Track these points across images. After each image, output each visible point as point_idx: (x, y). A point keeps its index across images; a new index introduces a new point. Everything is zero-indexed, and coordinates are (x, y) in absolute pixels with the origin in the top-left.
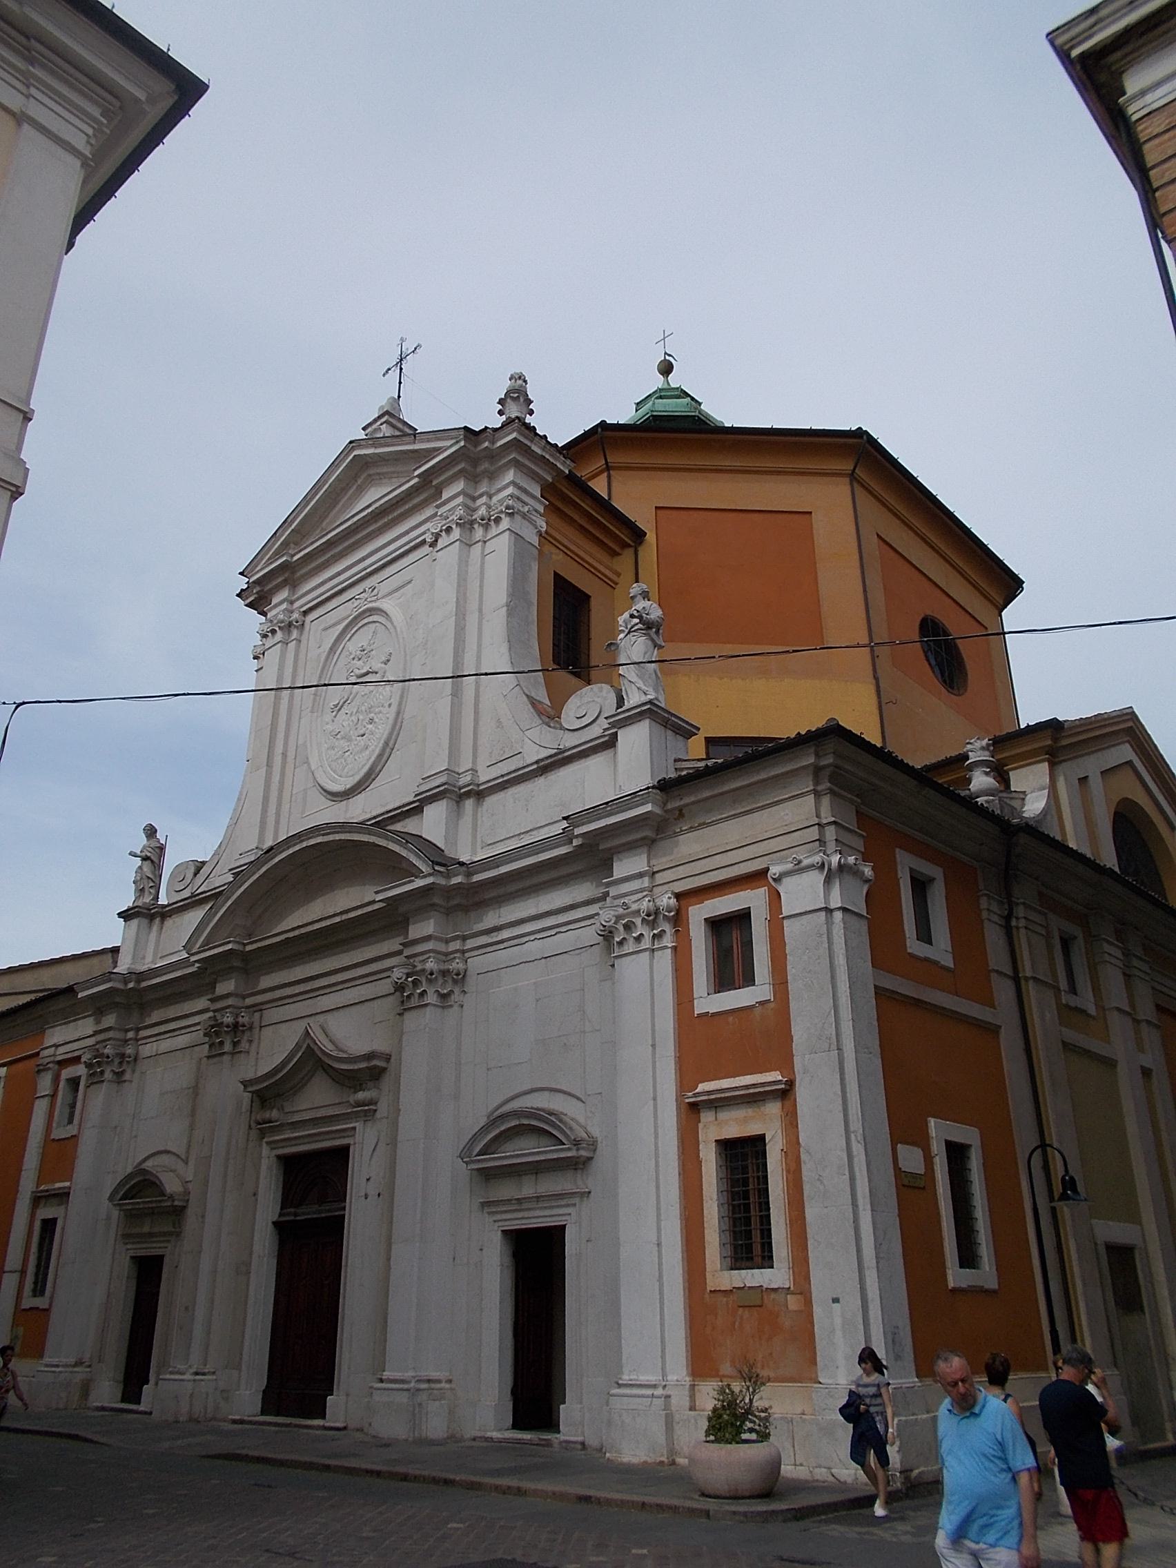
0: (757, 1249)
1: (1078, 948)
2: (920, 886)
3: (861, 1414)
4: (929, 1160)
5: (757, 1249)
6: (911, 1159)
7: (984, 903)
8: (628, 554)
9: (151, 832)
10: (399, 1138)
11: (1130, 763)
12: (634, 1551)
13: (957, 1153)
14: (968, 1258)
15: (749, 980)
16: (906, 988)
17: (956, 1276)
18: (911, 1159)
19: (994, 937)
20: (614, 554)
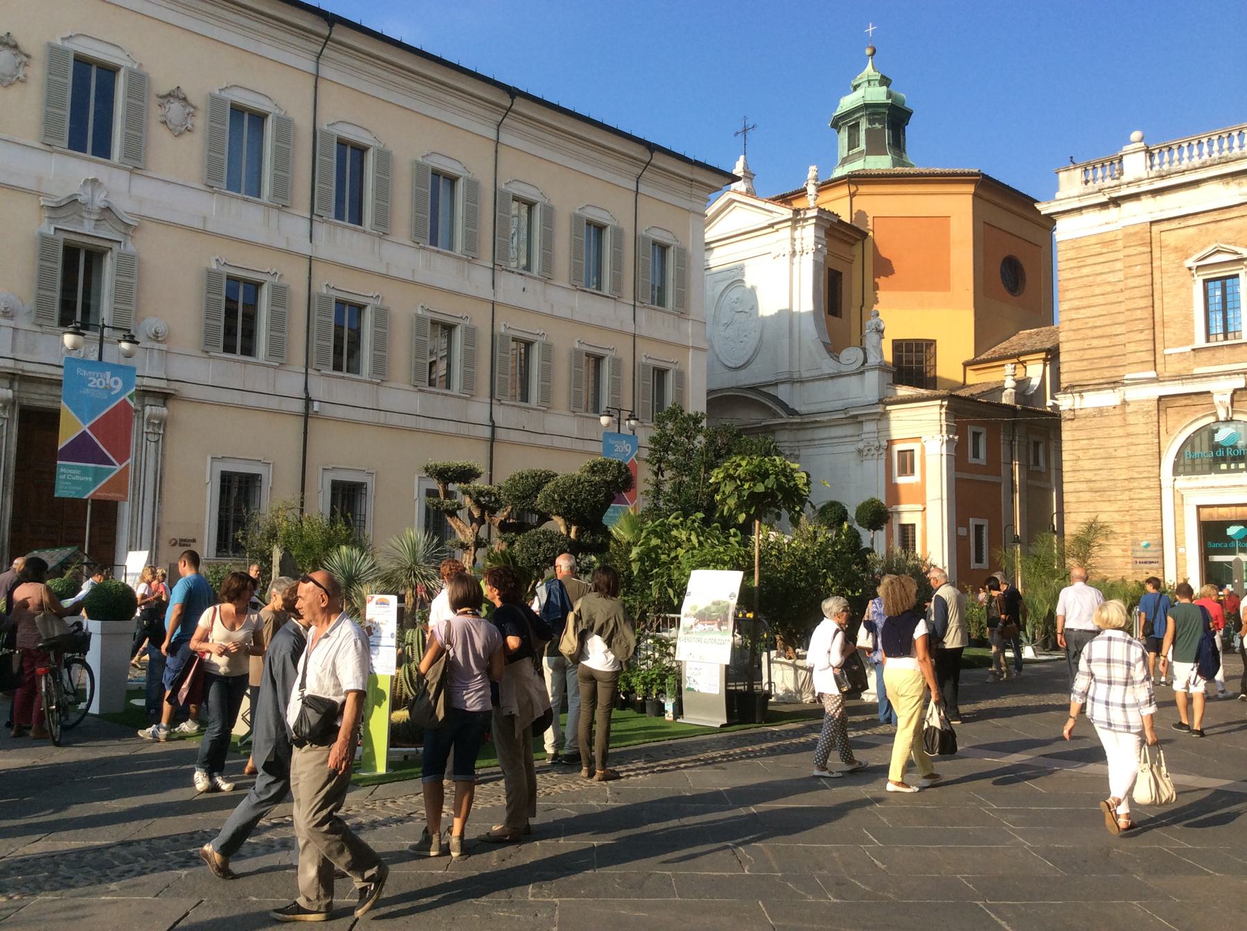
0: (235, 485)
1: (1041, 447)
2: (976, 435)
3: (1159, 705)
4: (968, 531)
5: (235, 485)
6: (962, 531)
7: (445, 782)
8: (860, 243)
9: (137, 343)
10: (1066, 510)
11: (1206, 281)
12: (883, 867)
13: (979, 529)
14: (979, 559)
15: (912, 472)
16: (966, 476)
17: (974, 565)
18: (962, 531)
19: (1004, 450)
20: (853, 245)
